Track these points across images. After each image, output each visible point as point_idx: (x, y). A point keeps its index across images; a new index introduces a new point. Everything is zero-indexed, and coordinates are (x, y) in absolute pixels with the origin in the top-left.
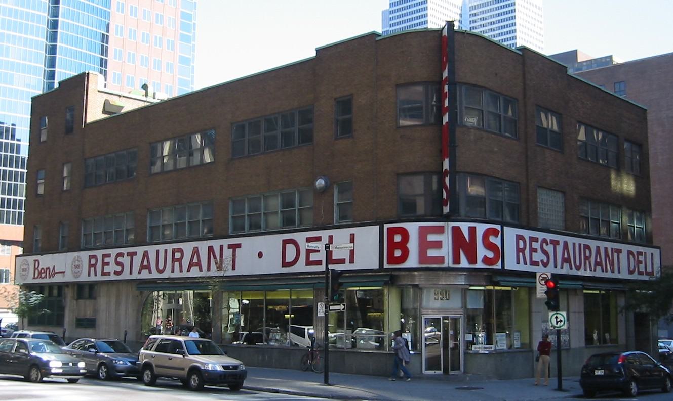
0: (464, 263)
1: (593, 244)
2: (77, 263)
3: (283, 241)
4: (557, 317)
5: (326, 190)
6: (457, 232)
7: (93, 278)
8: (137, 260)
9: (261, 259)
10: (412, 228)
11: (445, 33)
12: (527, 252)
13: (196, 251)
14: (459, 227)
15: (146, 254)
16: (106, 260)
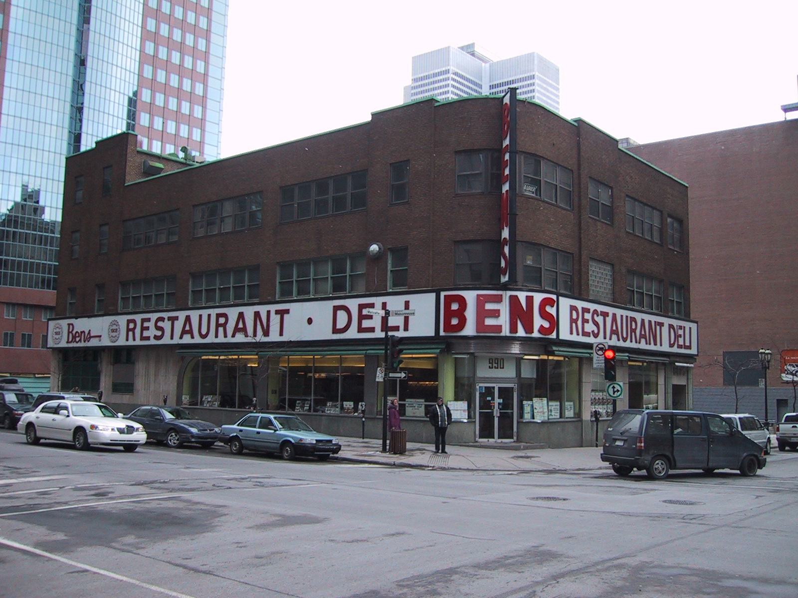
0: (521, 332)
1: (639, 316)
3: (128, 320)
4: (614, 387)
5: (378, 258)
6: (514, 300)
7: (131, 343)
8: (179, 325)
9: (311, 325)
10: (470, 296)
11: (507, 100)
12: (580, 322)
13: (241, 316)
15: (188, 319)
16: (146, 324)
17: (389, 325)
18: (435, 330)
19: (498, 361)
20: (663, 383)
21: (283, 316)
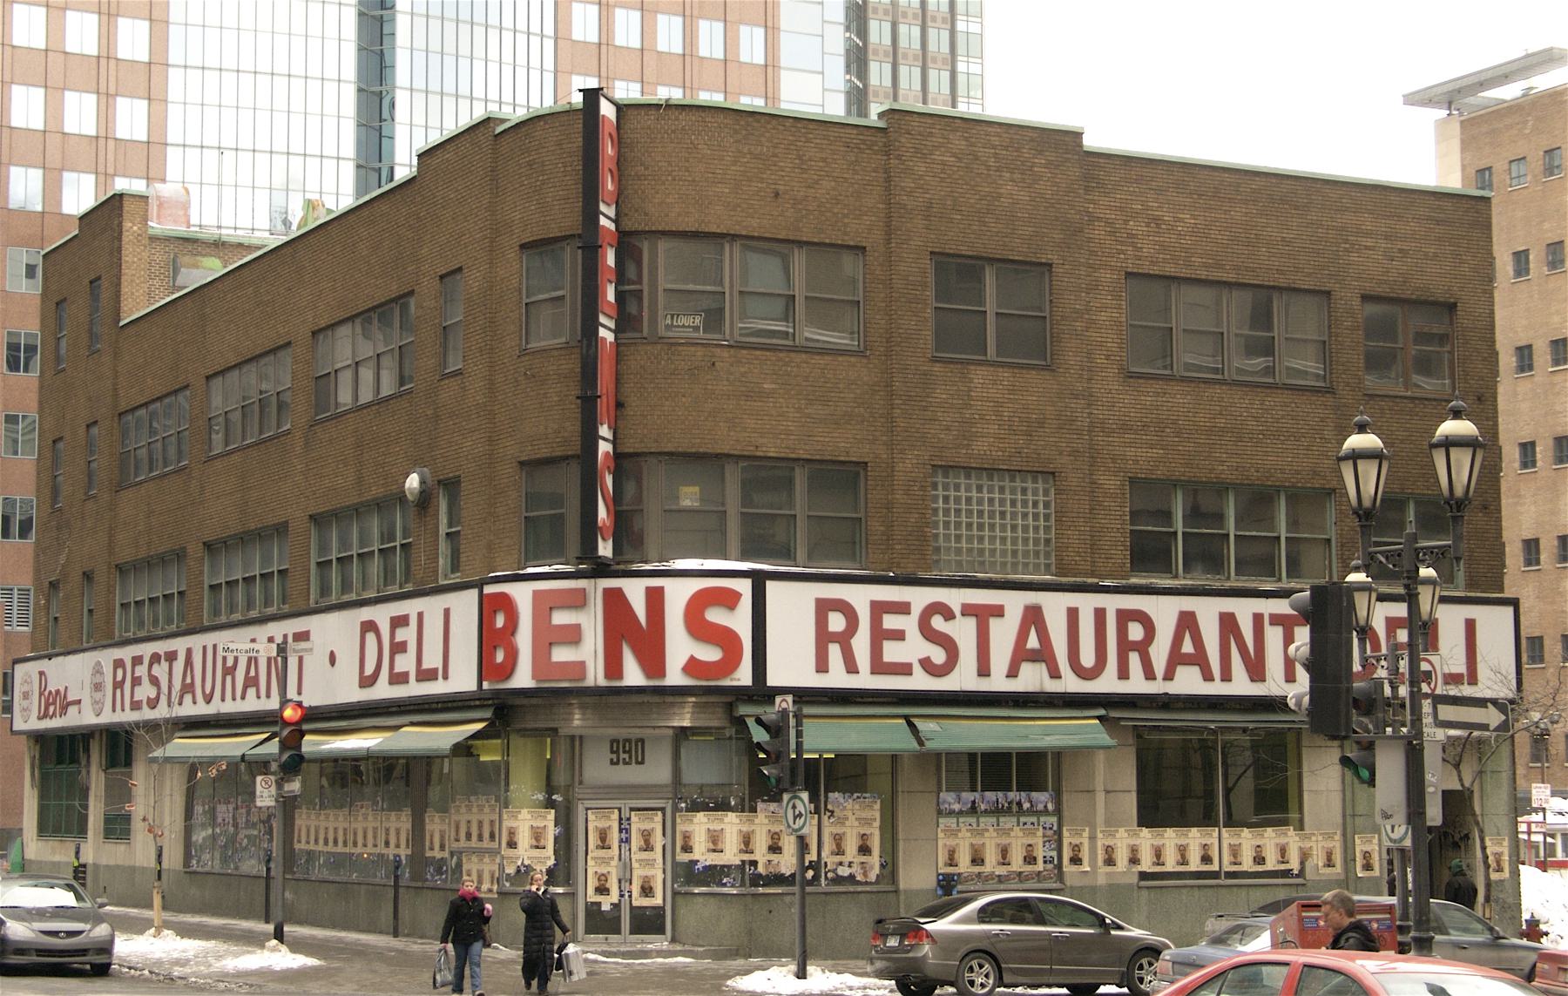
4: (794, 807)
8: (1003, 634)
10: (522, 594)
13: (1187, 622)
16: (890, 622)
17: (1406, 604)
18: (1221, 645)
20: (889, 770)
21: (1148, 653)
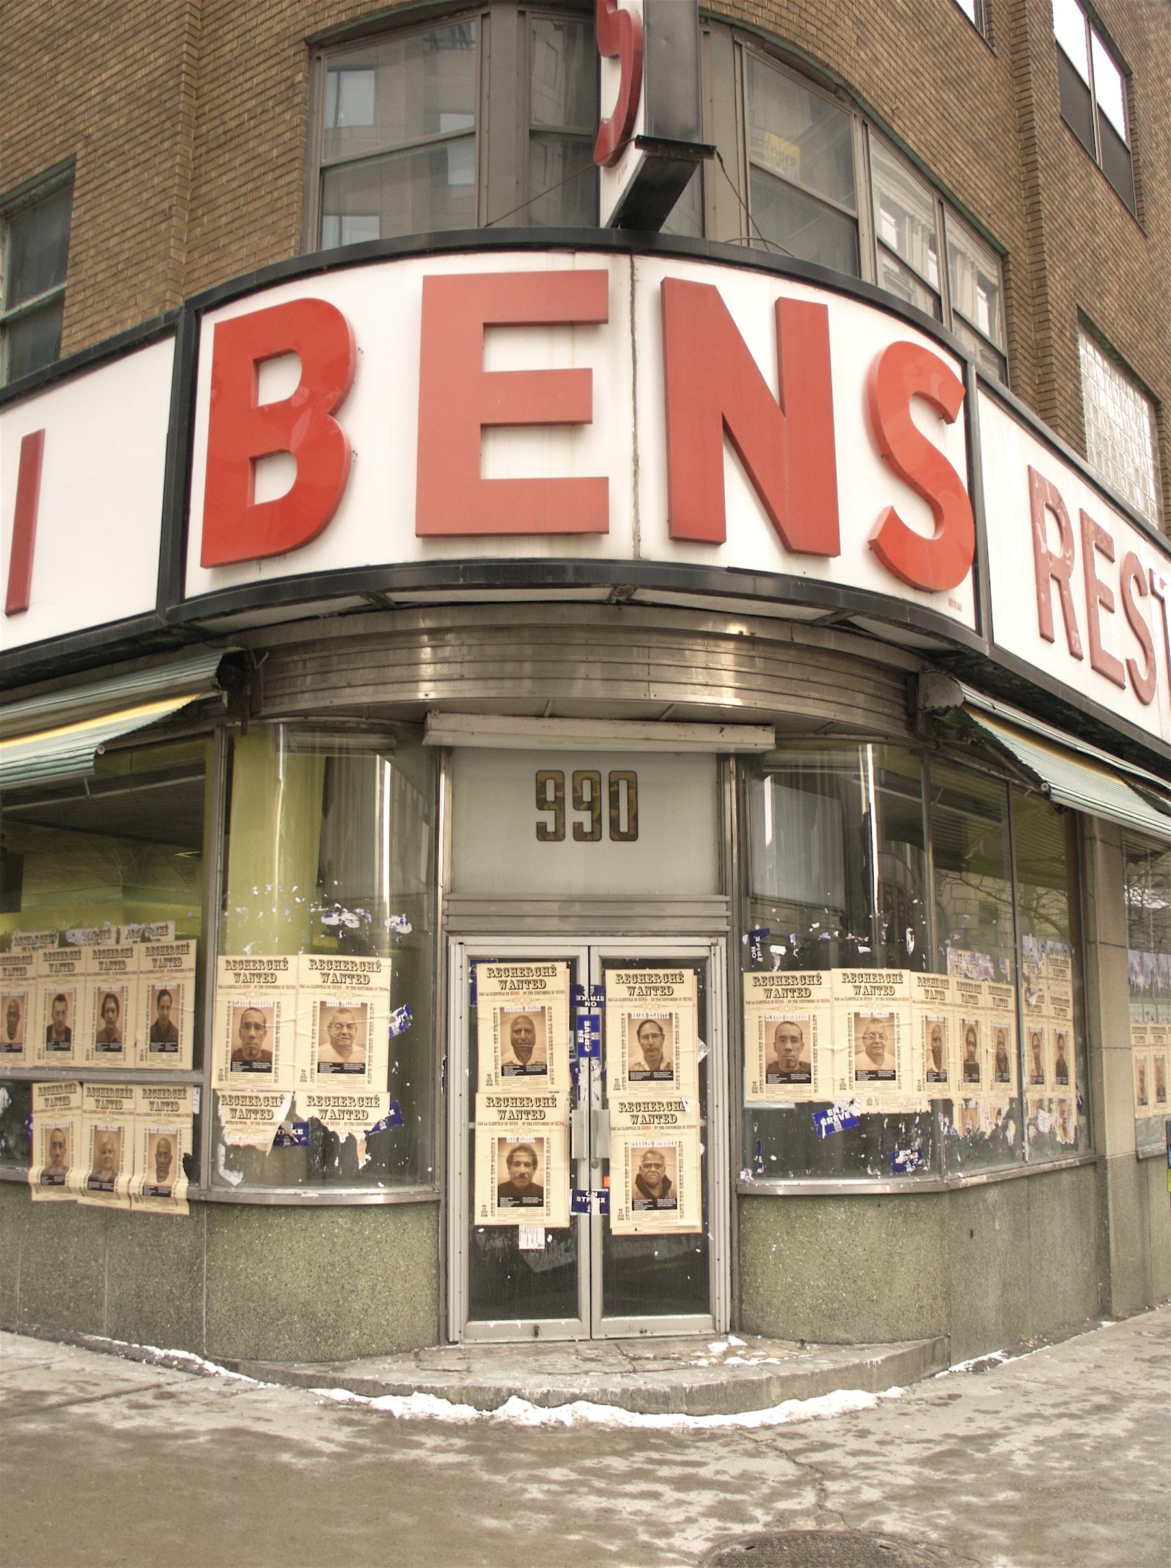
2: (936, 1035)
14: (709, 293)
19: (559, 787)
